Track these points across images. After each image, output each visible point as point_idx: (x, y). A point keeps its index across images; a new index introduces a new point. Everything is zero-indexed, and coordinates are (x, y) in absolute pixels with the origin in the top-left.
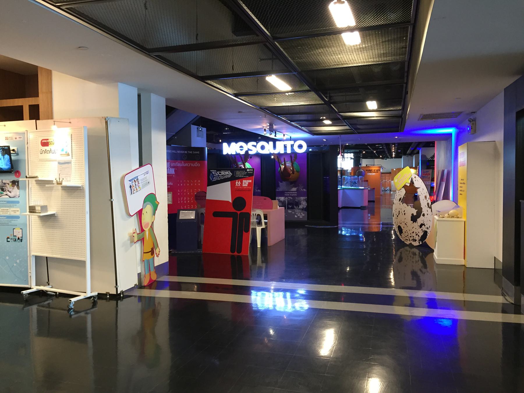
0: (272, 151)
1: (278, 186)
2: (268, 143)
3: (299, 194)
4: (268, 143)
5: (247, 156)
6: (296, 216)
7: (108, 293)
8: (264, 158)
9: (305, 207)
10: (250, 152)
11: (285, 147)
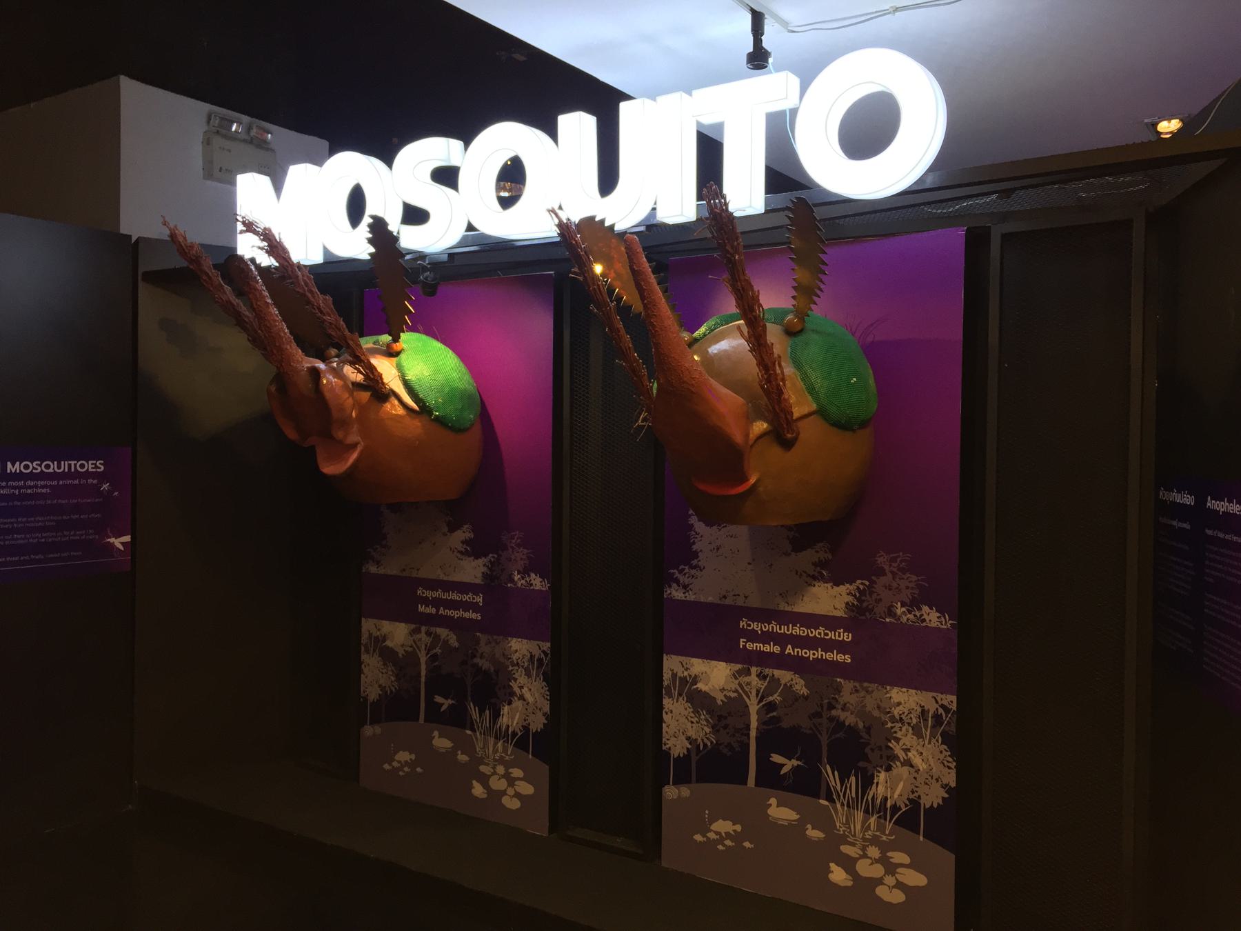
0: (583, 203)
1: (688, 557)
2: (552, 132)
3: (878, 651)
4: (552, 132)
5: (382, 289)
6: (838, 875)
7: (798, 434)
8: (555, 272)
9: (933, 797)
10: (412, 239)
11: (710, 152)
